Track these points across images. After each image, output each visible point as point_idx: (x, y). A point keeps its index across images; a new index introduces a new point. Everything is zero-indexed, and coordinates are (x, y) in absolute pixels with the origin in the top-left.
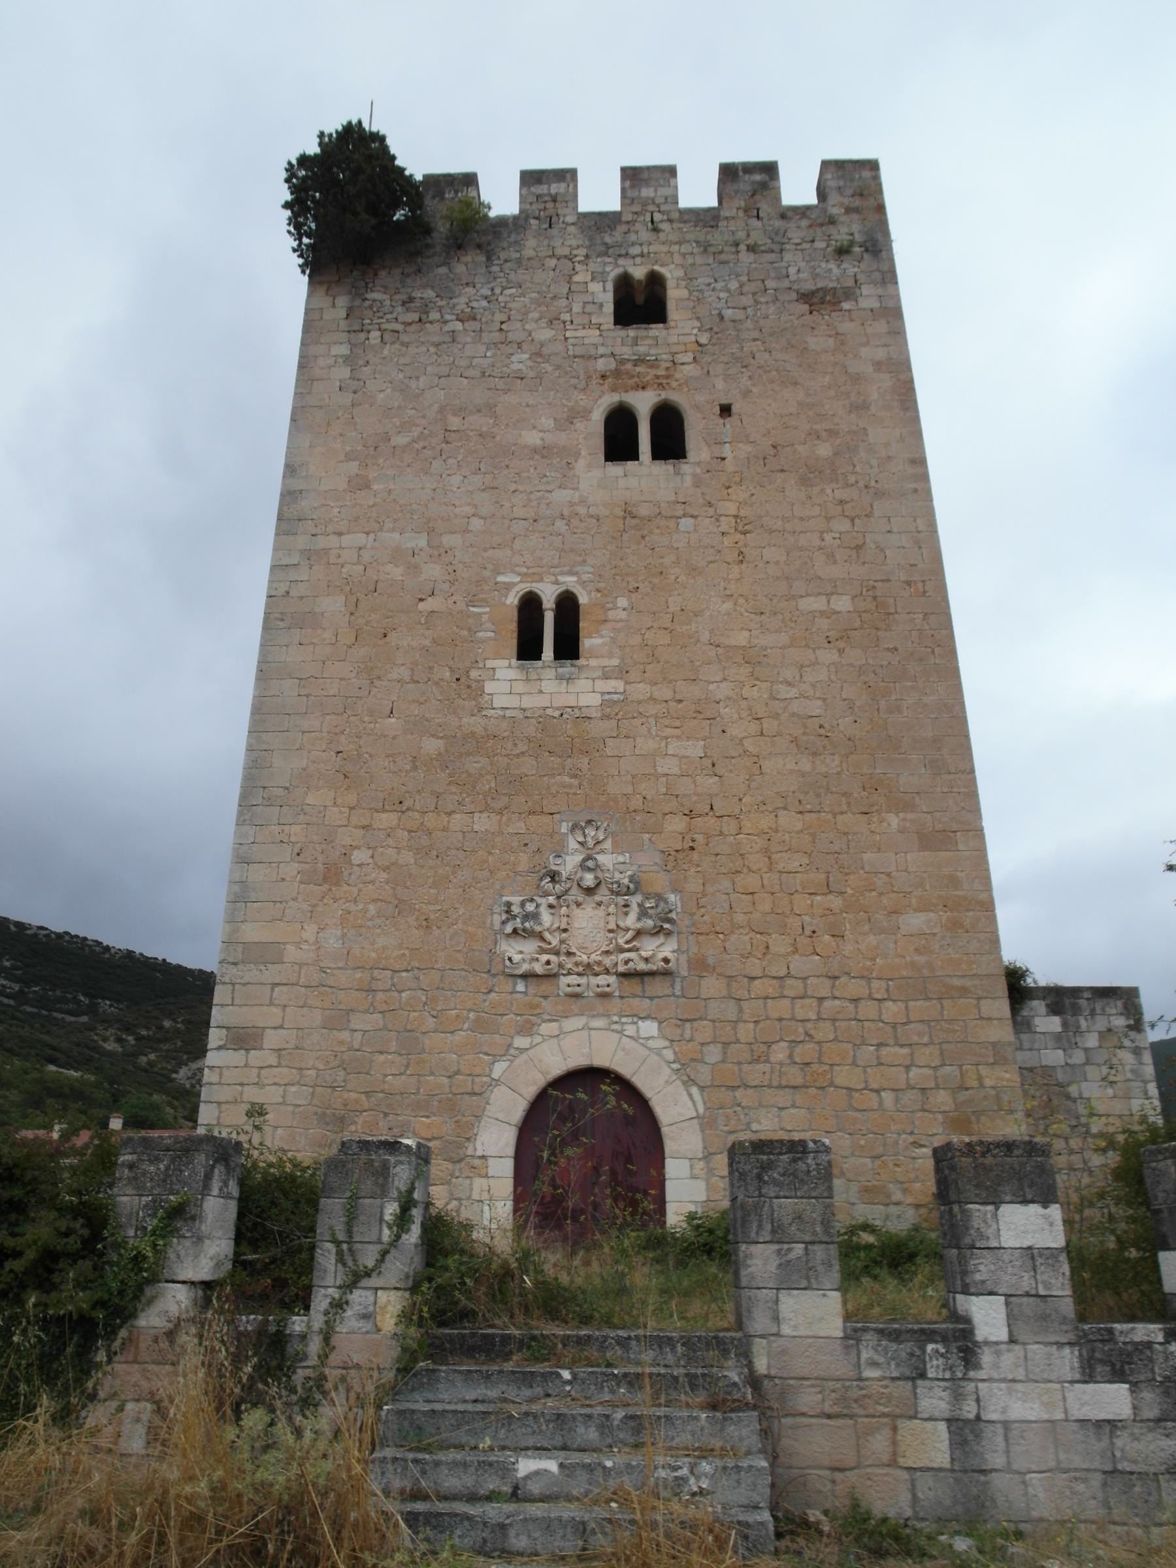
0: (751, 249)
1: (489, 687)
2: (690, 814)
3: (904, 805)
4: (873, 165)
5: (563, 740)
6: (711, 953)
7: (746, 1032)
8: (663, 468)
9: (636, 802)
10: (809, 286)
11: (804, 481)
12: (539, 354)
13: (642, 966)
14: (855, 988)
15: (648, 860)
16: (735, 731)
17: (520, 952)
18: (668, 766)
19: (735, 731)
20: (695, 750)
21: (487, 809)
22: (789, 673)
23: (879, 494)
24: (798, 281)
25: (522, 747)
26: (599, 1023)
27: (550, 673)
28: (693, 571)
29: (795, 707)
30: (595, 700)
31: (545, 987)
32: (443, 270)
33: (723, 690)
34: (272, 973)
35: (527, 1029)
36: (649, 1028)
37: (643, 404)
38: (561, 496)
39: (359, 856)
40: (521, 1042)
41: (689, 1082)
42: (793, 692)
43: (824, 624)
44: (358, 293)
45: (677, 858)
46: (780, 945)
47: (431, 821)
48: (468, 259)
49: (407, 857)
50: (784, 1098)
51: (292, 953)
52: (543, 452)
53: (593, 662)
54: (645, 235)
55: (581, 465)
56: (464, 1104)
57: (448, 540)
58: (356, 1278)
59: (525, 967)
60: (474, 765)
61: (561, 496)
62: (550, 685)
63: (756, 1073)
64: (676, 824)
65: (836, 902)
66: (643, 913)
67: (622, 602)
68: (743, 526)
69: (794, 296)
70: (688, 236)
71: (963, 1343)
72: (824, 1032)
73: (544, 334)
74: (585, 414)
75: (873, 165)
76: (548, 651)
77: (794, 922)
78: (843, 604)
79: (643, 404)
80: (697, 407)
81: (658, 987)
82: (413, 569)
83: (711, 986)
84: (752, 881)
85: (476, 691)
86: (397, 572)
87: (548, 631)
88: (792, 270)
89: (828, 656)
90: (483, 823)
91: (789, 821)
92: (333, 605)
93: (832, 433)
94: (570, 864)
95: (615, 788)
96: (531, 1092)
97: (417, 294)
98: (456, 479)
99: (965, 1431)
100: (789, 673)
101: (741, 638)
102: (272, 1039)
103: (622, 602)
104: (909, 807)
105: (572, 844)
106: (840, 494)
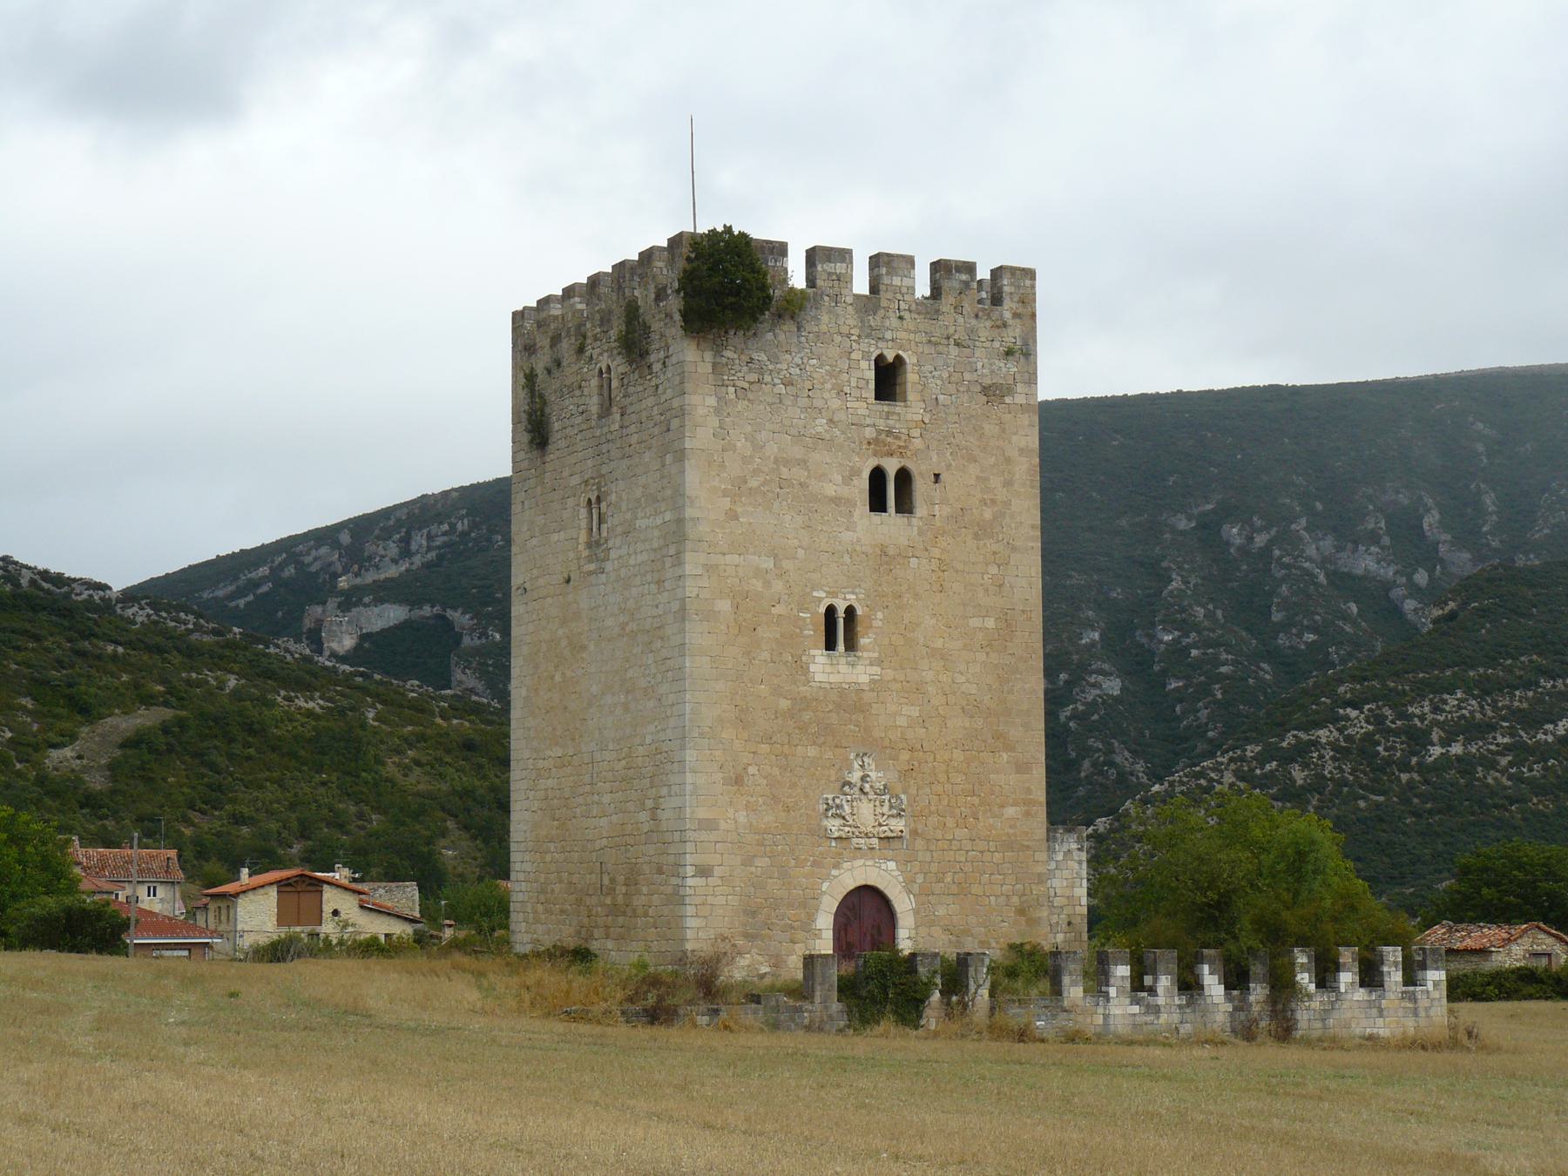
0: (957, 344)
1: (812, 668)
2: (912, 750)
3: (1010, 748)
4: (1030, 274)
5: (851, 702)
6: (920, 828)
7: (934, 867)
8: (901, 520)
9: (887, 742)
10: (987, 381)
11: (976, 536)
12: (831, 421)
13: (889, 834)
14: (982, 845)
15: (892, 776)
16: (935, 702)
17: (833, 825)
18: (901, 721)
19: (935, 702)
20: (915, 712)
21: (814, 743)
22: (962, 667)
23: (1014, 549)
24: (983, 375)
25: (831, 707)
26: (870, 863)
27: (843, 660)
28: (917, 596)
29: (963, 688)
30: (864, 679)
31: (845, 843)
32: (770, 336)
33: (929, 676)
34: (713, 836)
35: (837, 866)
36: (892, 865)
37: (891, 467)
38: (848, 536)
39: (752, 770)
40: (835, 872)
41: (909, 892)
42: (963, 679)
43: (980, 635)
44: (718, 351)
45: (908, 772)
46: (950, 823)
47: (786, 749)
48: (785, 328)
49: (776, 771)
50: (950, 899)
51: (723, 825)
52: (836, 500)
53: (865, 655)
54: (895, 322)
55: (857, 513)
56: (809, 906)
57: (787, 564)
58: (979, 986)
59: (836, 835)
60: (807, 716)
61: (848, 536)
62: (843, 668)
63: (938, 888)
64: (905, 756)
65: (976, 800)
66: (891, 807)
67: (880, 615)
68: (943, 567)
69: (979, 388)
70: (921, 327)
71: (1107, 998)
72: (968, 868)
73: (835, 403)
74: (858, 473)
75: (1030, 274)
76: (841, 646)
77: (958, 811)
78: (990, 623)
79: (891, 467)
80: (921, 474)
81: (896, 844)
82: (767, 584)
83: (920, 843)
84: (939, 788)
85: (805, 670)
86: (758, 585)
87: (839, 629)
88: (979, 365)
89: (981, 656)
90: (812, 752)
91: (958, 755)
92: (724, 606)
93: (993, 501)
94: (855, 777)
95: (877, 733)
96: (840, 898)
97: (755, 356)
98: (788, 517)
99: (1106, 1017)
100: (962, 667)
101: (939, 644)
102: (717, 871)
103: (880, 615)
104: (1013, 749)
105: (1256, 1009)
106: (995, 547)
